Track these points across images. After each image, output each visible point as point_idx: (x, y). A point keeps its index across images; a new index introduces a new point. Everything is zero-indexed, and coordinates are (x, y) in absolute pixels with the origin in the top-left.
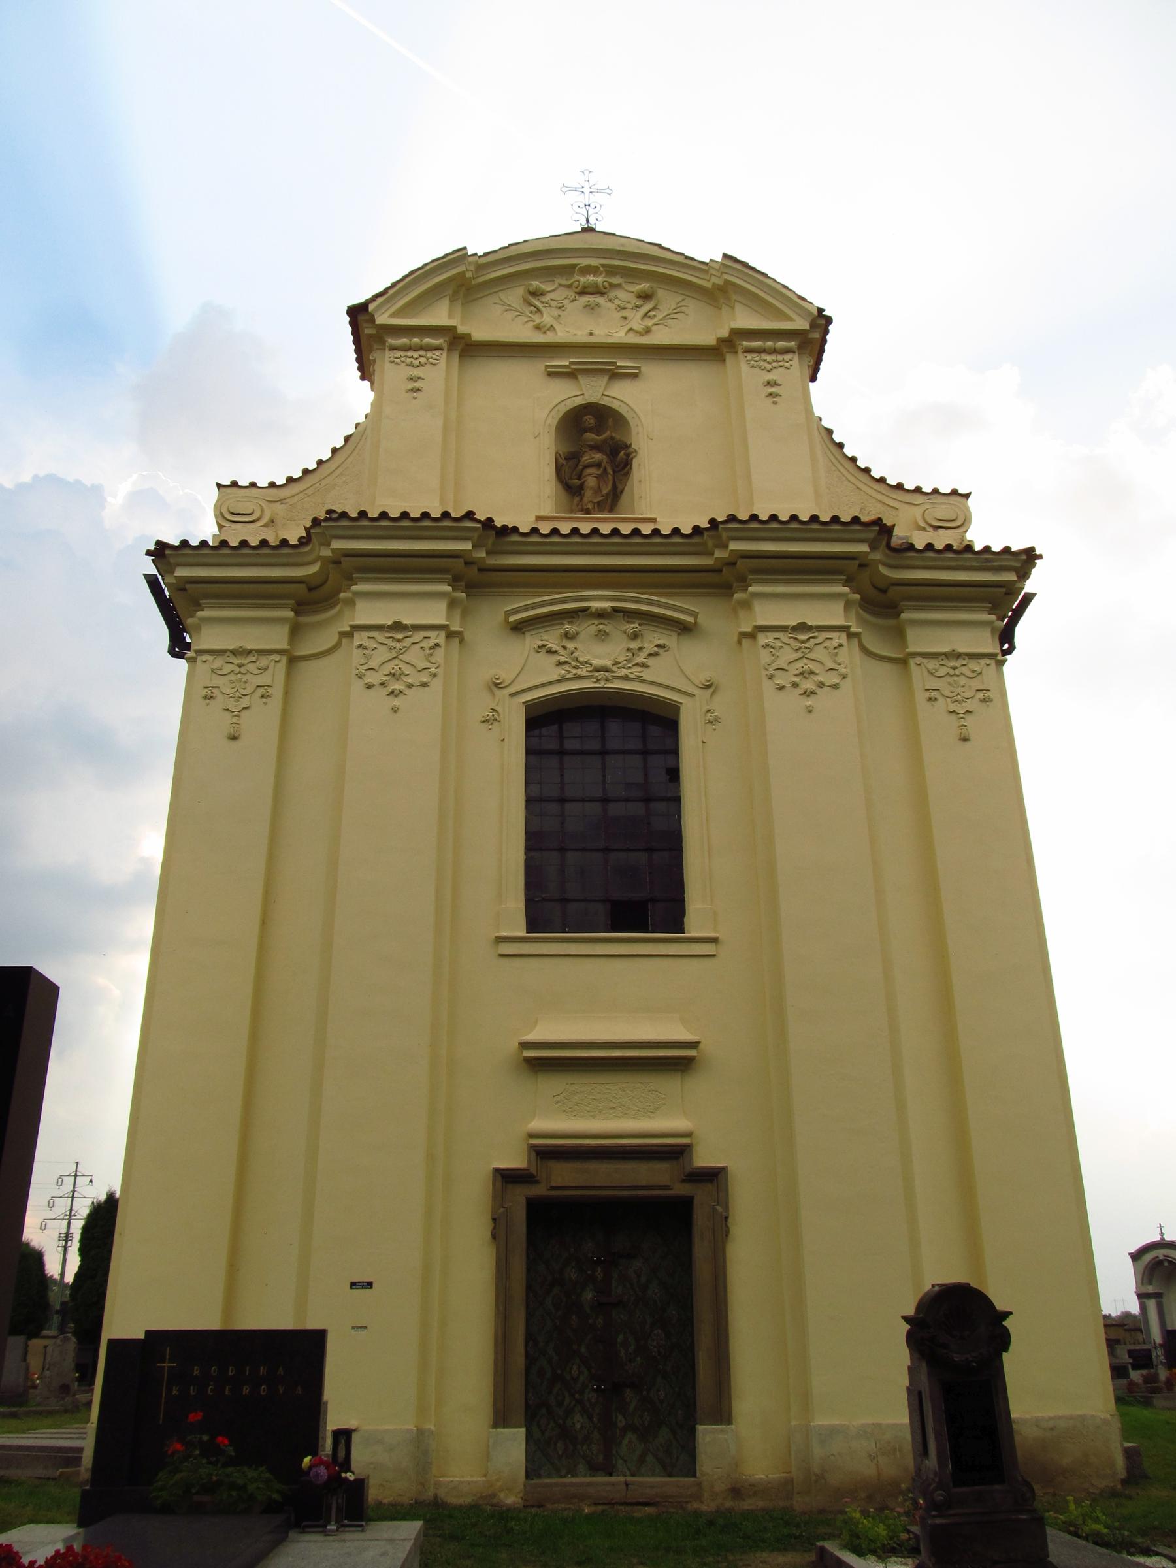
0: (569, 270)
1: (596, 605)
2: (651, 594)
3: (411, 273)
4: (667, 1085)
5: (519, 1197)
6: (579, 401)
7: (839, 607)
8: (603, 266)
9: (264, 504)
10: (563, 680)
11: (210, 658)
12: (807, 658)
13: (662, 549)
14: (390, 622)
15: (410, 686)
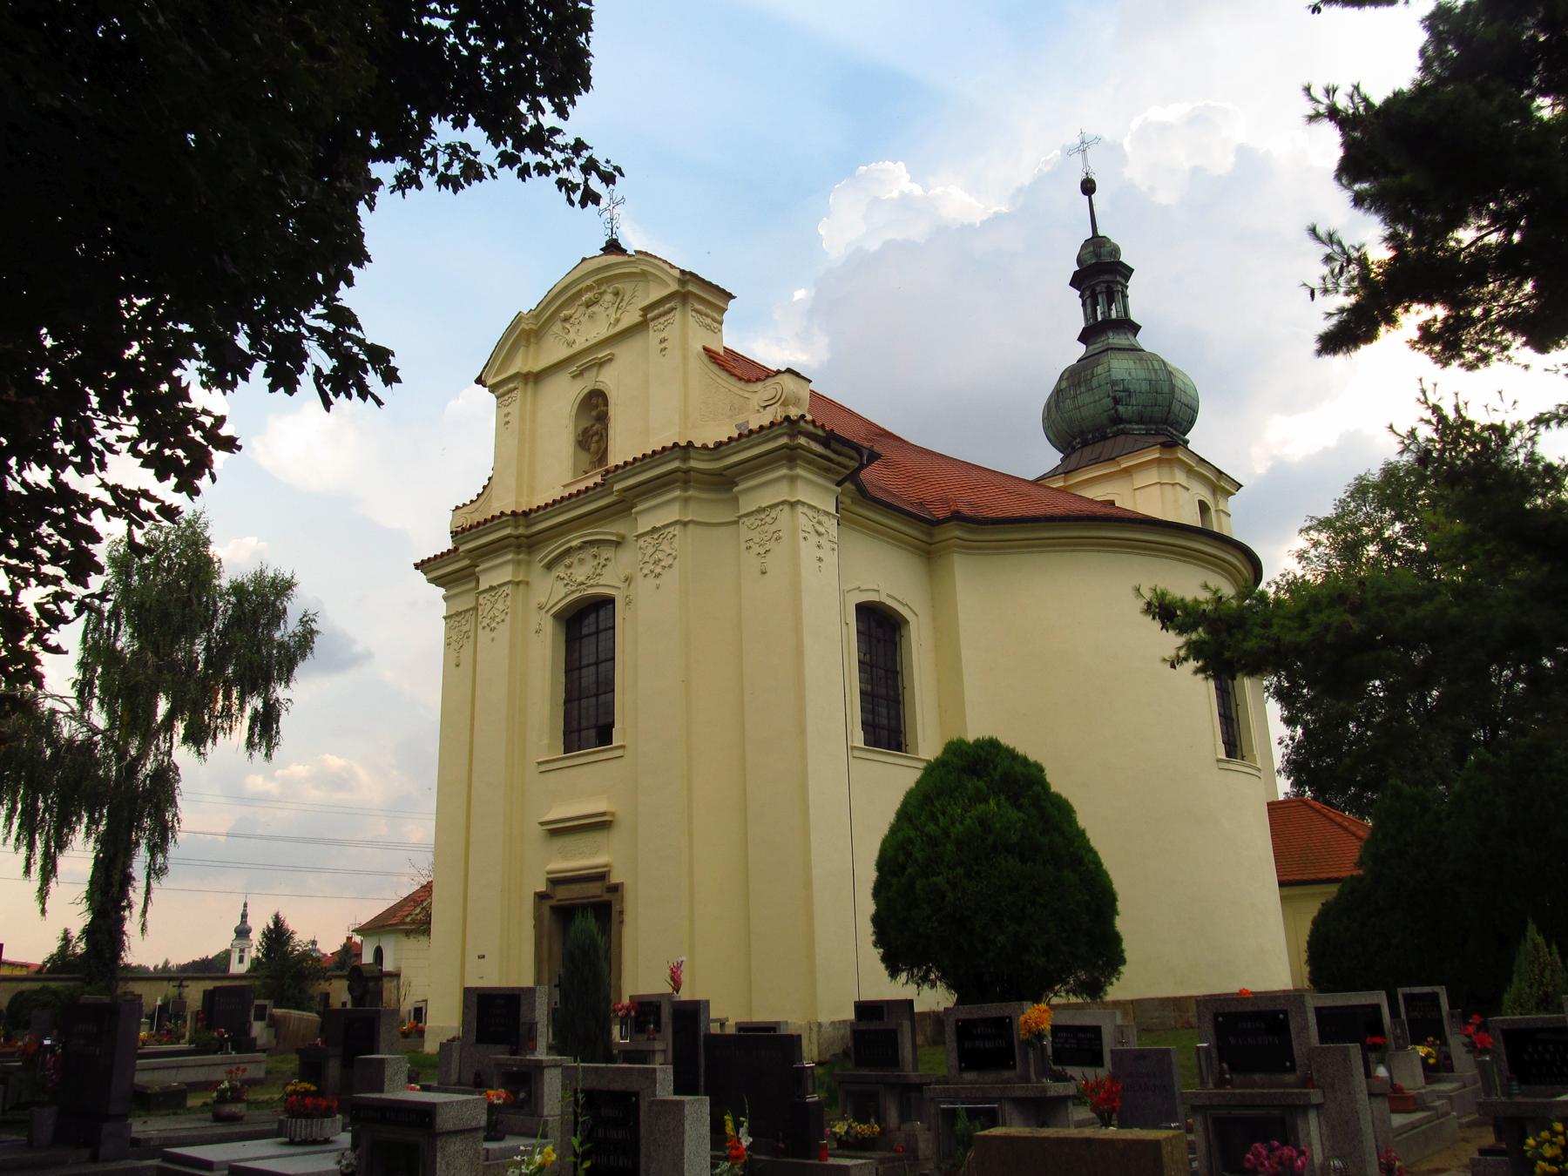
0: (579, 294)
1: (574, 543)
2: (591, 529)
3: (498, 344)
4: (599, 837)
5: (547, 904)
6: (586, 391)
7: (509, 569)
8: (594, 282)
9: (467, 516)
10: (567, 595)
11: (746, 519)
12: (746, 515)
13: (561, 510)
14: (650, 528)
15: (498, 623)
